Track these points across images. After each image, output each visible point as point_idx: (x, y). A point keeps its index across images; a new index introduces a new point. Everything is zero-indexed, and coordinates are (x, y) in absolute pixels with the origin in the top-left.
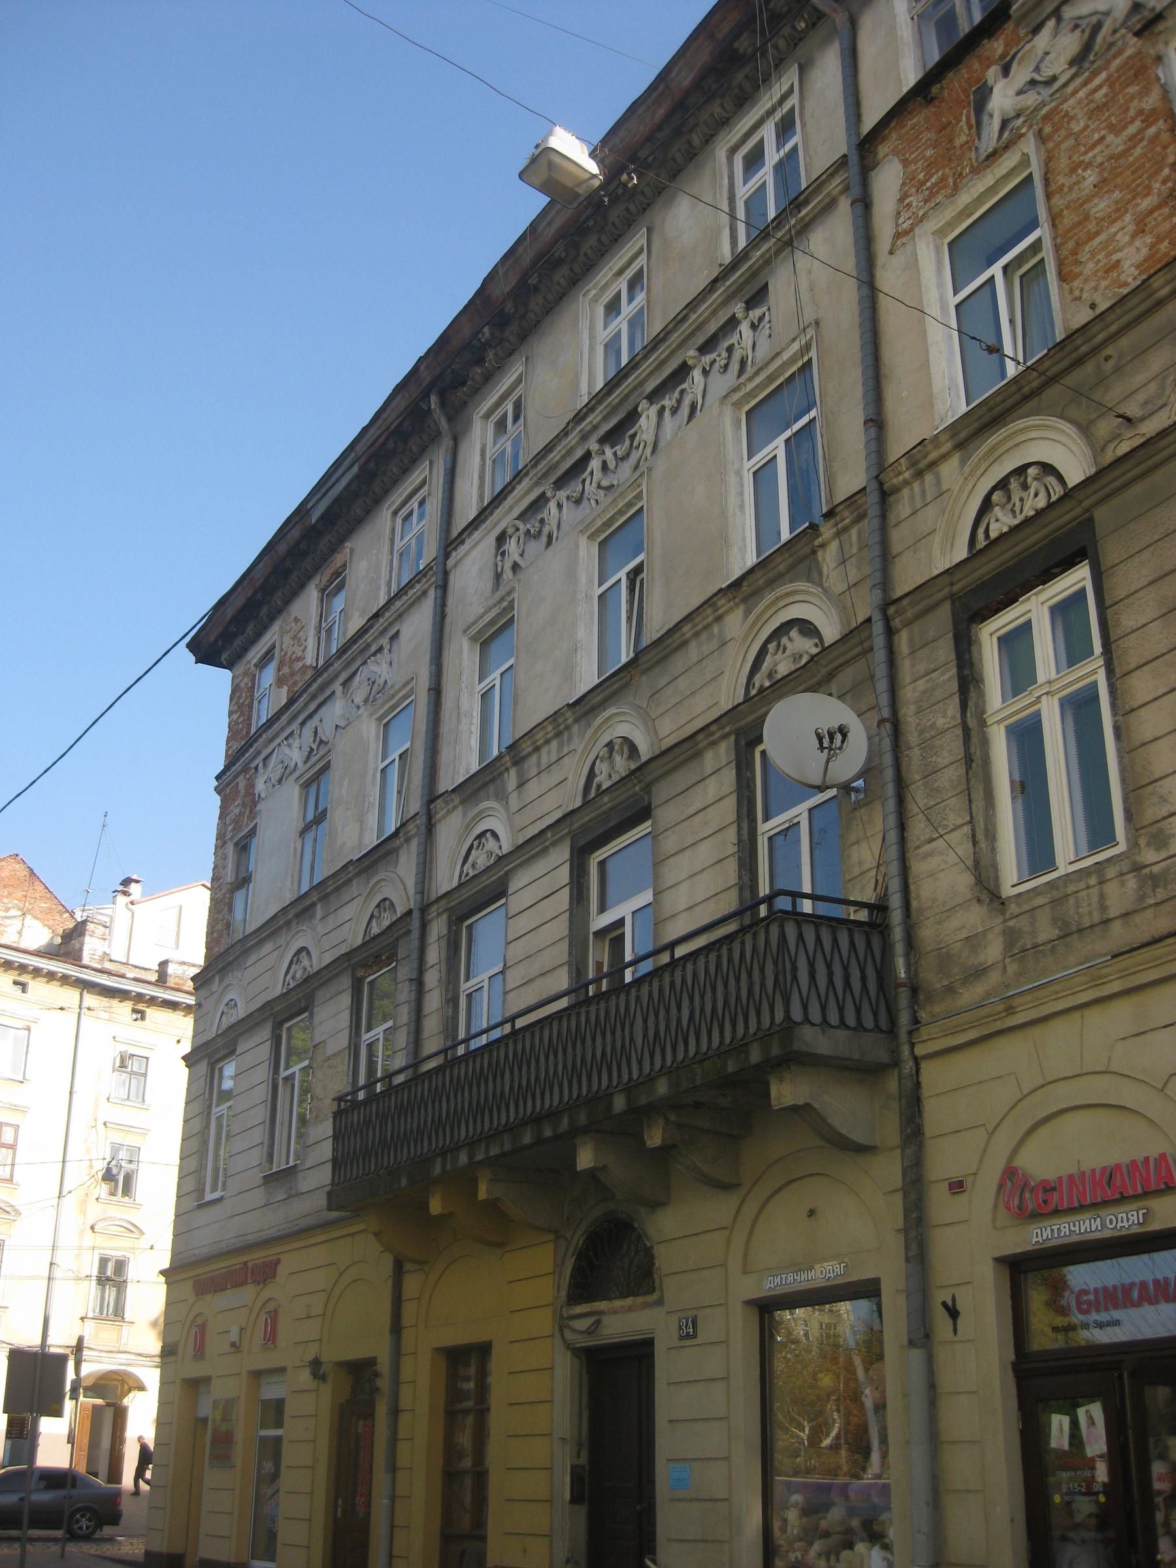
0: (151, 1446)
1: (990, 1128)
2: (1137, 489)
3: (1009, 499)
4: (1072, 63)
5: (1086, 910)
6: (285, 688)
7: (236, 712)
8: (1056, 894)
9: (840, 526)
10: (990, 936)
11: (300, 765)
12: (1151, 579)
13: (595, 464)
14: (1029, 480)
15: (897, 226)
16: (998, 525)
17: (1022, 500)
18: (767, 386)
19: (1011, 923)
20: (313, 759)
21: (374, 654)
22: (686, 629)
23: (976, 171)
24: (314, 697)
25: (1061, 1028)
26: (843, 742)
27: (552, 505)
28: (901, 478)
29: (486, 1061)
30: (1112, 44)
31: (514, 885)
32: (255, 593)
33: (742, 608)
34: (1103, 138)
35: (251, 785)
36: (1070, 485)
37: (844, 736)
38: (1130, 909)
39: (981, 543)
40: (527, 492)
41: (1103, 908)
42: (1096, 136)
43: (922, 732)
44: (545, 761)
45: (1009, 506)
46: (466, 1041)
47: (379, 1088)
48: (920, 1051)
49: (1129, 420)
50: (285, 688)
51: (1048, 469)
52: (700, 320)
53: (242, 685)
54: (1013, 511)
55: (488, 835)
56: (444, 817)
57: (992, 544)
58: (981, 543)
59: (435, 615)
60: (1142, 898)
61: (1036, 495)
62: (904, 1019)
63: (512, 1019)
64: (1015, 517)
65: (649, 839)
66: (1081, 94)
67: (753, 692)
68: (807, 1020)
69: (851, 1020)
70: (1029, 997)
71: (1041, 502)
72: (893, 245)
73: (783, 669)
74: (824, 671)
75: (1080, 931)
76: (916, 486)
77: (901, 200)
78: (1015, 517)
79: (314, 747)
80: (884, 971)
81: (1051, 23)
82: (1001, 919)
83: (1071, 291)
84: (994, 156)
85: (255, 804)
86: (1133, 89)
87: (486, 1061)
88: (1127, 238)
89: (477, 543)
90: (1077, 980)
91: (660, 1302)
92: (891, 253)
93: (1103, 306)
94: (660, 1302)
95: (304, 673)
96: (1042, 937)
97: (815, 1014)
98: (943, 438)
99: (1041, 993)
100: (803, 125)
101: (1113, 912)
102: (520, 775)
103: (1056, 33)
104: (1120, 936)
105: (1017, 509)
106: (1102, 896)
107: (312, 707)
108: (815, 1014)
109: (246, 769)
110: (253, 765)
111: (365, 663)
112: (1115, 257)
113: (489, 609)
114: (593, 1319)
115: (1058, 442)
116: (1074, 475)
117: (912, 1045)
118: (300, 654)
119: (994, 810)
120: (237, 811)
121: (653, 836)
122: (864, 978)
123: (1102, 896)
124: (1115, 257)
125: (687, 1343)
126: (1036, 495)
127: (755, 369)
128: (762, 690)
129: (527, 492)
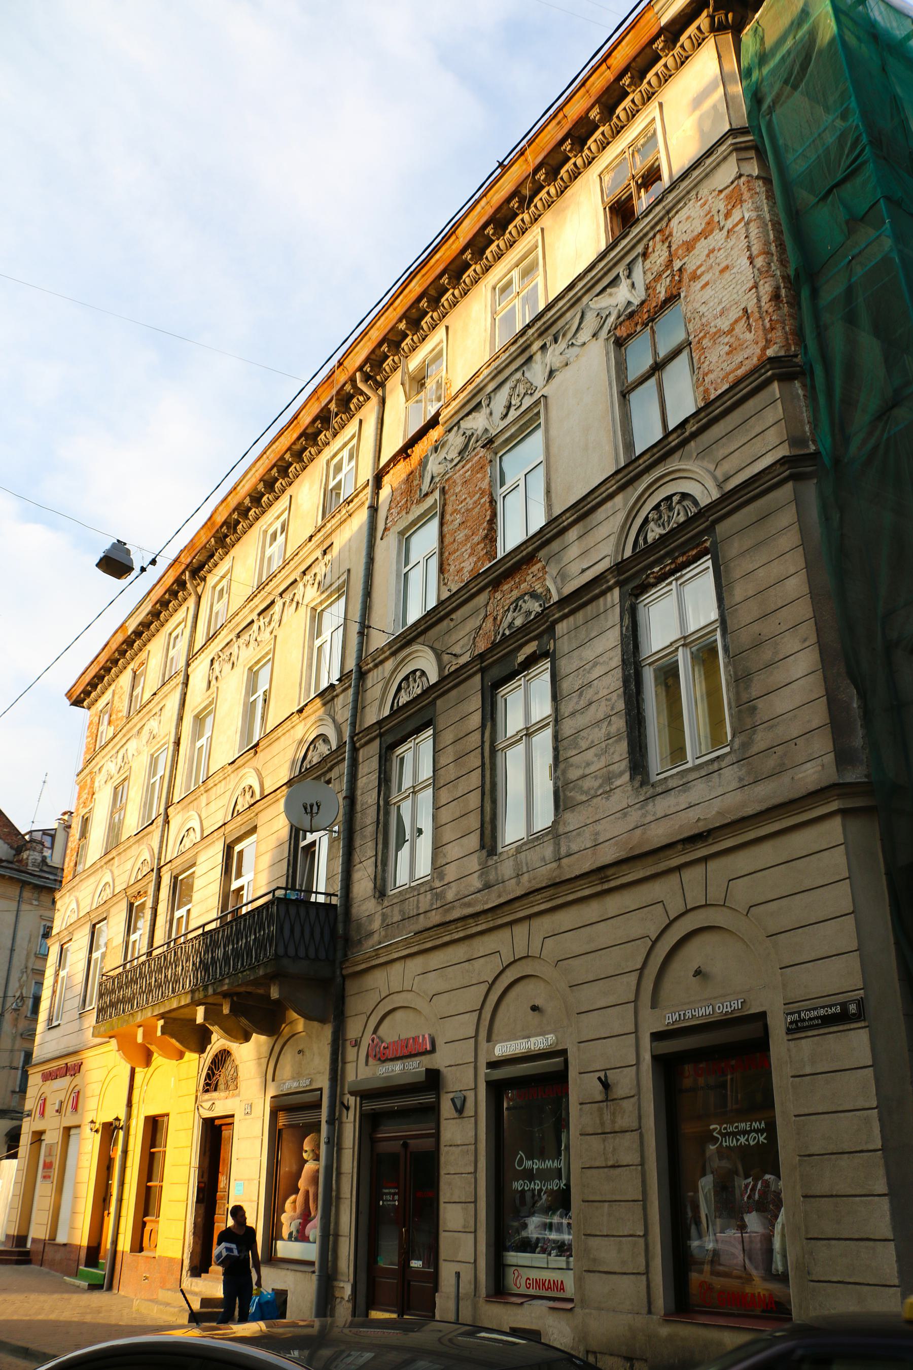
0: (736, 1177)
1: (368, 1014)
2: (454, 693)
3: (660, 517)
4: (459, 453)
5: (410, 908)
6: (112, 728)
7: (89, 737)
8: (402, 898)
9: (376, 661)
10: (377, 916)
11: (116, 774)
12: (453, 741)
13: (255, 626)
14: (674, 504)
15: (386, 524)
16: (654, 534)
17: (669, 517)
18: (328, 600)
19: (384, 910)
20: (122, 772)
21: (153, 716)
22: (512, 554)
23: (419, 502)
24: (124, 736)
25: (398, 967)
26: (318, 809)
27: (236, 646)
28: (369, 666)
29: (220, 935)
30: (475, 448)
31: (200, 859)
32: (100, 669)
33: (303, 723)
34: (466, 499)
35: (93, 782)
36: (702, 505)
37: (319, 807)
38: (427, 910)
39: (395, 708)
40: (226, 637)
41: (418, 908)
42: (463, 497)
43: (362, 805)
44: (219, 793)
45: (660, 522)
46: (137, 958)
47: (128, 966)
48: (345, 972)
49: (455, 655)
50: (112, 728)
51: (684, 496)
52: (478, 380)
53: (94, 721)
54: (663, 525)
55: (192, 830)
56: (174, 816)
57: (400, 709)
58: (395, 708)
59: (181, 699)
60: (432, 904)
61: (678, 514)
62: (339, 954)
63: (204, 926)
64: (664, 528)
65: (255, 844)
66: (461, 472)
67: (303, 770)
68: (286, 954)
69: (312, 954)
70: (384, 950)
71: (682, 519)
72: (383, 534)
73: (315, 761)
74: (329, 765)
75: (409, 918)
76: (375, 671)
77: (389, 510)
78: (664, 528)
79: (123, 765)
80: (333, 930)
81: (456, 428)
82: (380, 908)
83: (444, 579)
84: (426, 495)
85: (94, 794)
86: (479, 475)
87: (220, 935)
88: (467, 556)
89: (202, 661)
90: (401, 944)
91: (238, 1095)
92: (382, 539)
93: (454, 590)
94: (238, 1095)
95: (122, 720)
96: (395, 919)
97: (291, 952)
98: (385, 649)
99: (390, 948)
100: (357, 456)
101: (421, 911)
102: (208, 798)
103: (456, 435)
104: (422, 923)
105: (666, 524)
106: (418, 901)
107: (124, 741)
108: (291, 952)
109: (91, 773)
110: (94, 771)
111: (149, 720)
112: (462, 565)
113: (203, 702)
114: (211, 1103)
115: (692, 479)
116: (704, 501)
117: (342, 969)
118: (121, 708)
119: (387, 850)
120: (85, 796)
121: (257, 842)
122: (322, 933)
123: (418, 901)
124: (462, 565)
125: (247, 1117)
126: (678, 514)
127: (325, 587)
128: (307, 769)
129: (226, 637)
